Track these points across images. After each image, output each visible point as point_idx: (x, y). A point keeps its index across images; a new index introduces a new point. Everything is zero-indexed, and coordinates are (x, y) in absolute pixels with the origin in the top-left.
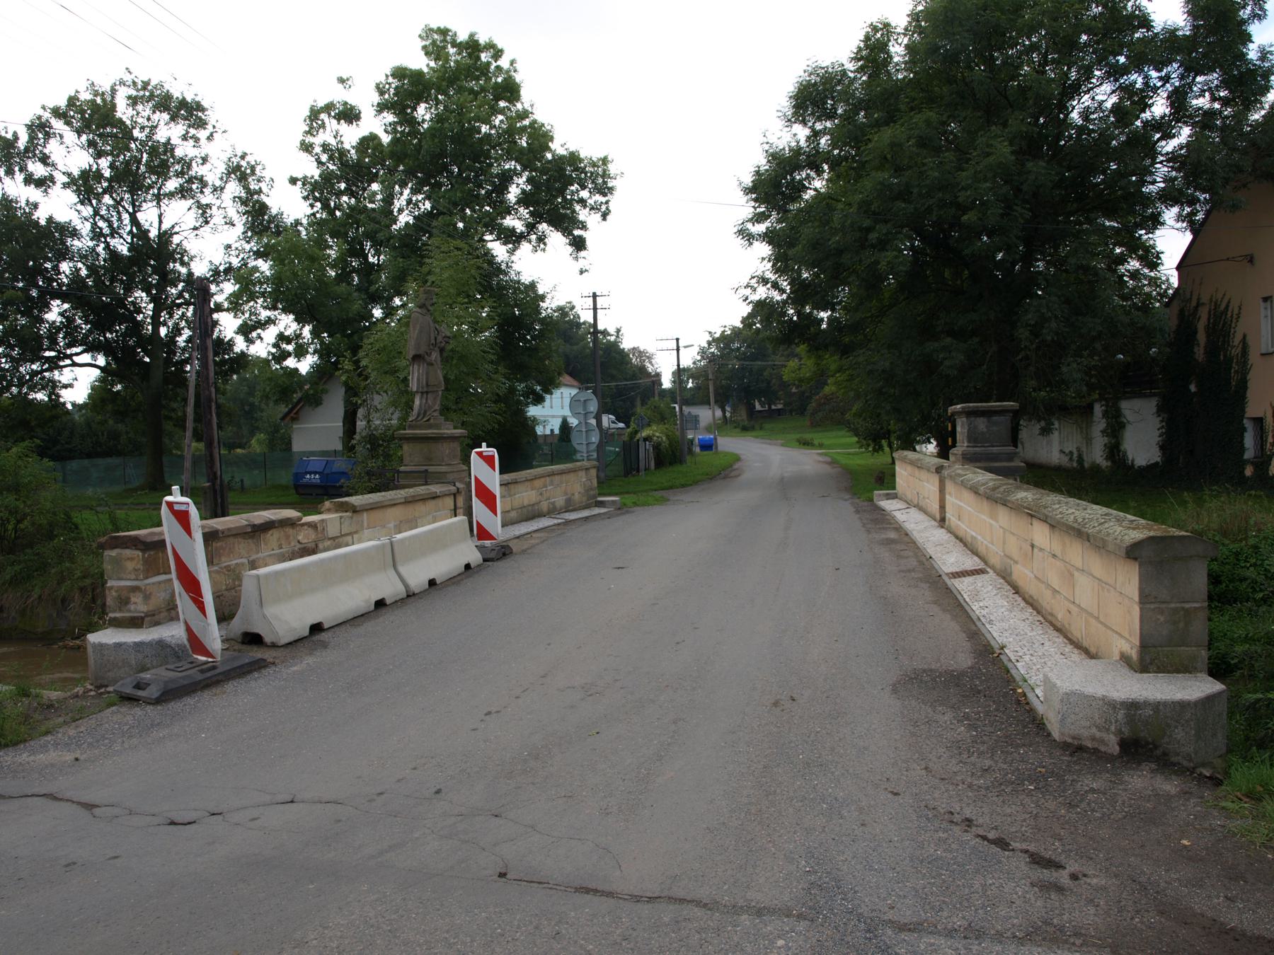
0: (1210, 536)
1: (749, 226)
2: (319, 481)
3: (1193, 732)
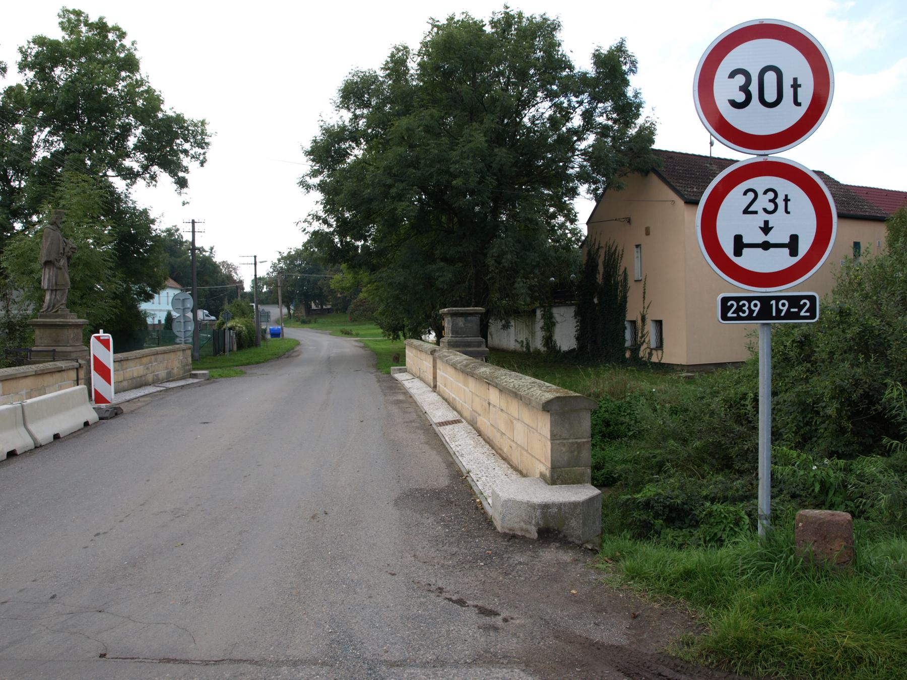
0: (604, 396)
1: (307, 178)
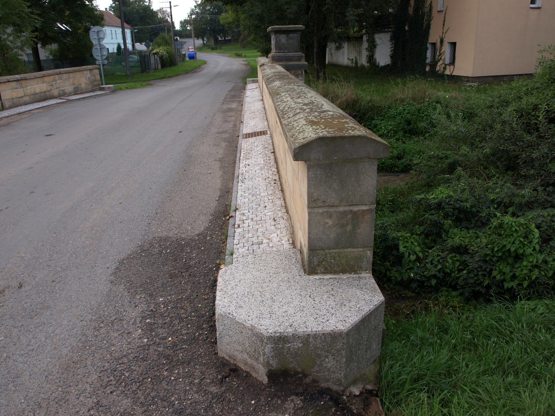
0: (408, 101)
3: (344, 360)
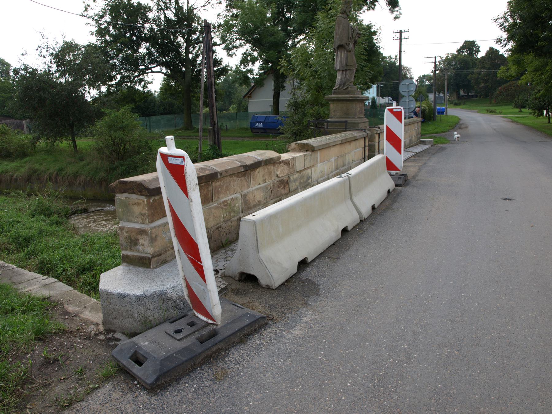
2: (262, 126)
